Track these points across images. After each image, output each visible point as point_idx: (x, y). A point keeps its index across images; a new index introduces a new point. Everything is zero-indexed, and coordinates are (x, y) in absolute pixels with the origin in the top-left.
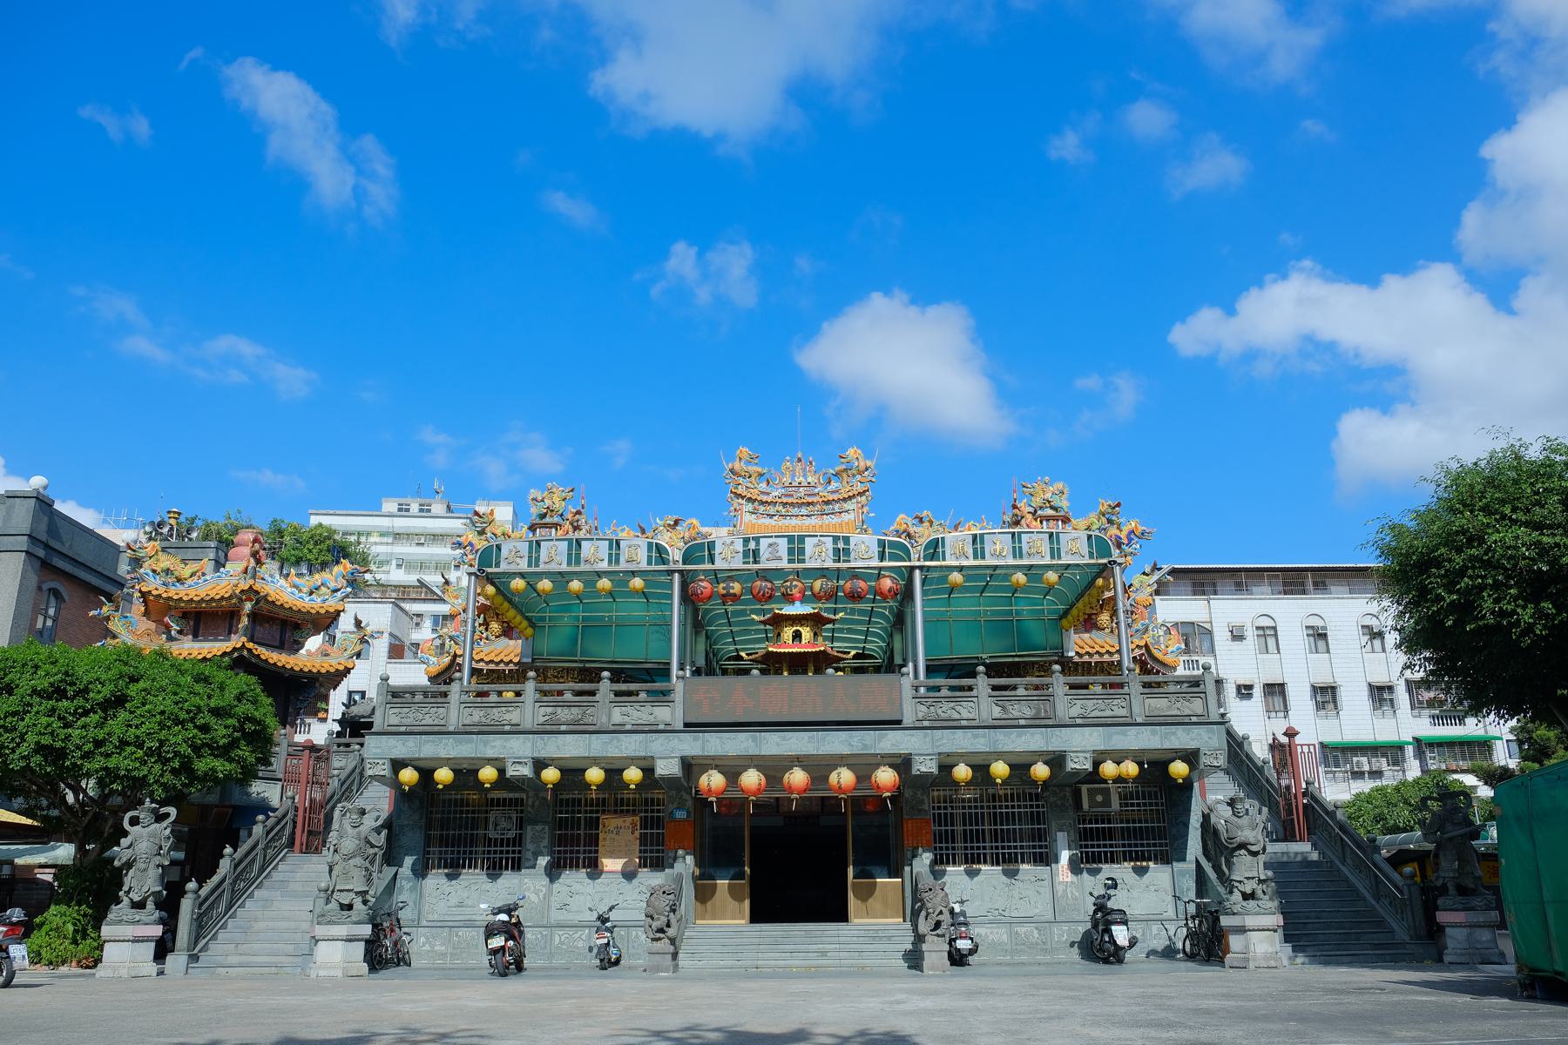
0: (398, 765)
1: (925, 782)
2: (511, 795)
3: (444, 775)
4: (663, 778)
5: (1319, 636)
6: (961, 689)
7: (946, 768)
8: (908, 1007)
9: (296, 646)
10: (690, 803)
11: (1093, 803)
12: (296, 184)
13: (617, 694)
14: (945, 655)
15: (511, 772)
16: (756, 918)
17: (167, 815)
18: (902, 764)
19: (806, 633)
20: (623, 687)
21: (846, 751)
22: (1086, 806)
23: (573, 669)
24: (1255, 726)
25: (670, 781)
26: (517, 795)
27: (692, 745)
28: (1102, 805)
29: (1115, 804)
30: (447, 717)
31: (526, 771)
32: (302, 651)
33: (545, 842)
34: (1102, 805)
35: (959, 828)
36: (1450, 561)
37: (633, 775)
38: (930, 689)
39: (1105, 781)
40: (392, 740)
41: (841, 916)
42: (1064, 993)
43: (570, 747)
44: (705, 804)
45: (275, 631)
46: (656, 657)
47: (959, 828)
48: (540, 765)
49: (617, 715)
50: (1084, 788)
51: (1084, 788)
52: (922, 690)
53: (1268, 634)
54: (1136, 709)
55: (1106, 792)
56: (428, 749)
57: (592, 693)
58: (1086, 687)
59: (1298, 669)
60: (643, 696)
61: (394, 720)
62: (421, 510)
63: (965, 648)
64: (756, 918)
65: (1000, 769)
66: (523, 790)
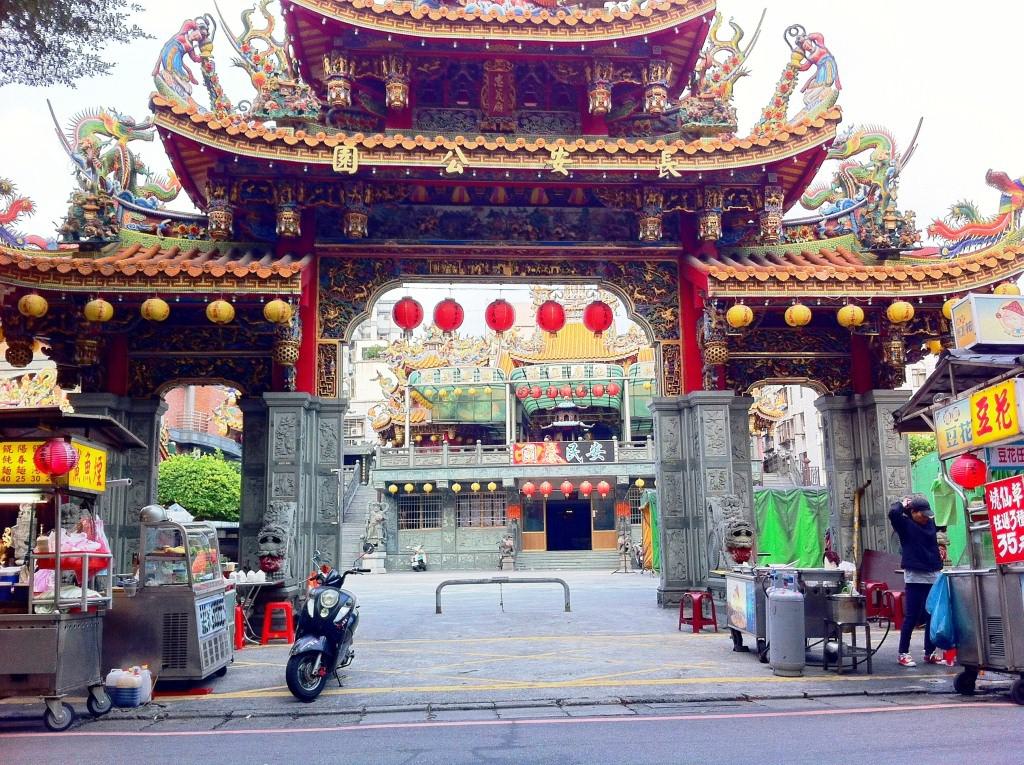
0: (388, 484)
1: (624, 487)
3: (409, 488)
5: (89, 455)
6: (640, 446)
7: (633, 479)
12: (12, 293)
13: (485, 450)
15: (439, 486)
16: (550, 548)
18: (612, 479)
19: (571, 416)
21: (588, 474)
25: (510, 489)
27: (518, 473)
30: (408, 462)
31: (446, 485)
33: (453, 516)
36: (899, 356)
37: (428, 487)
40: (385, 473)
41: (587, 546)
43: (465, 475)
48: (452, 482)
49: (485, 461)
54: (445, 461)
56: (401, 477)
57: (644, 445)
58: (459, 450)
60: (496, 450)
61: (385, 464)
64: (550, 548)
65: (409, 488)
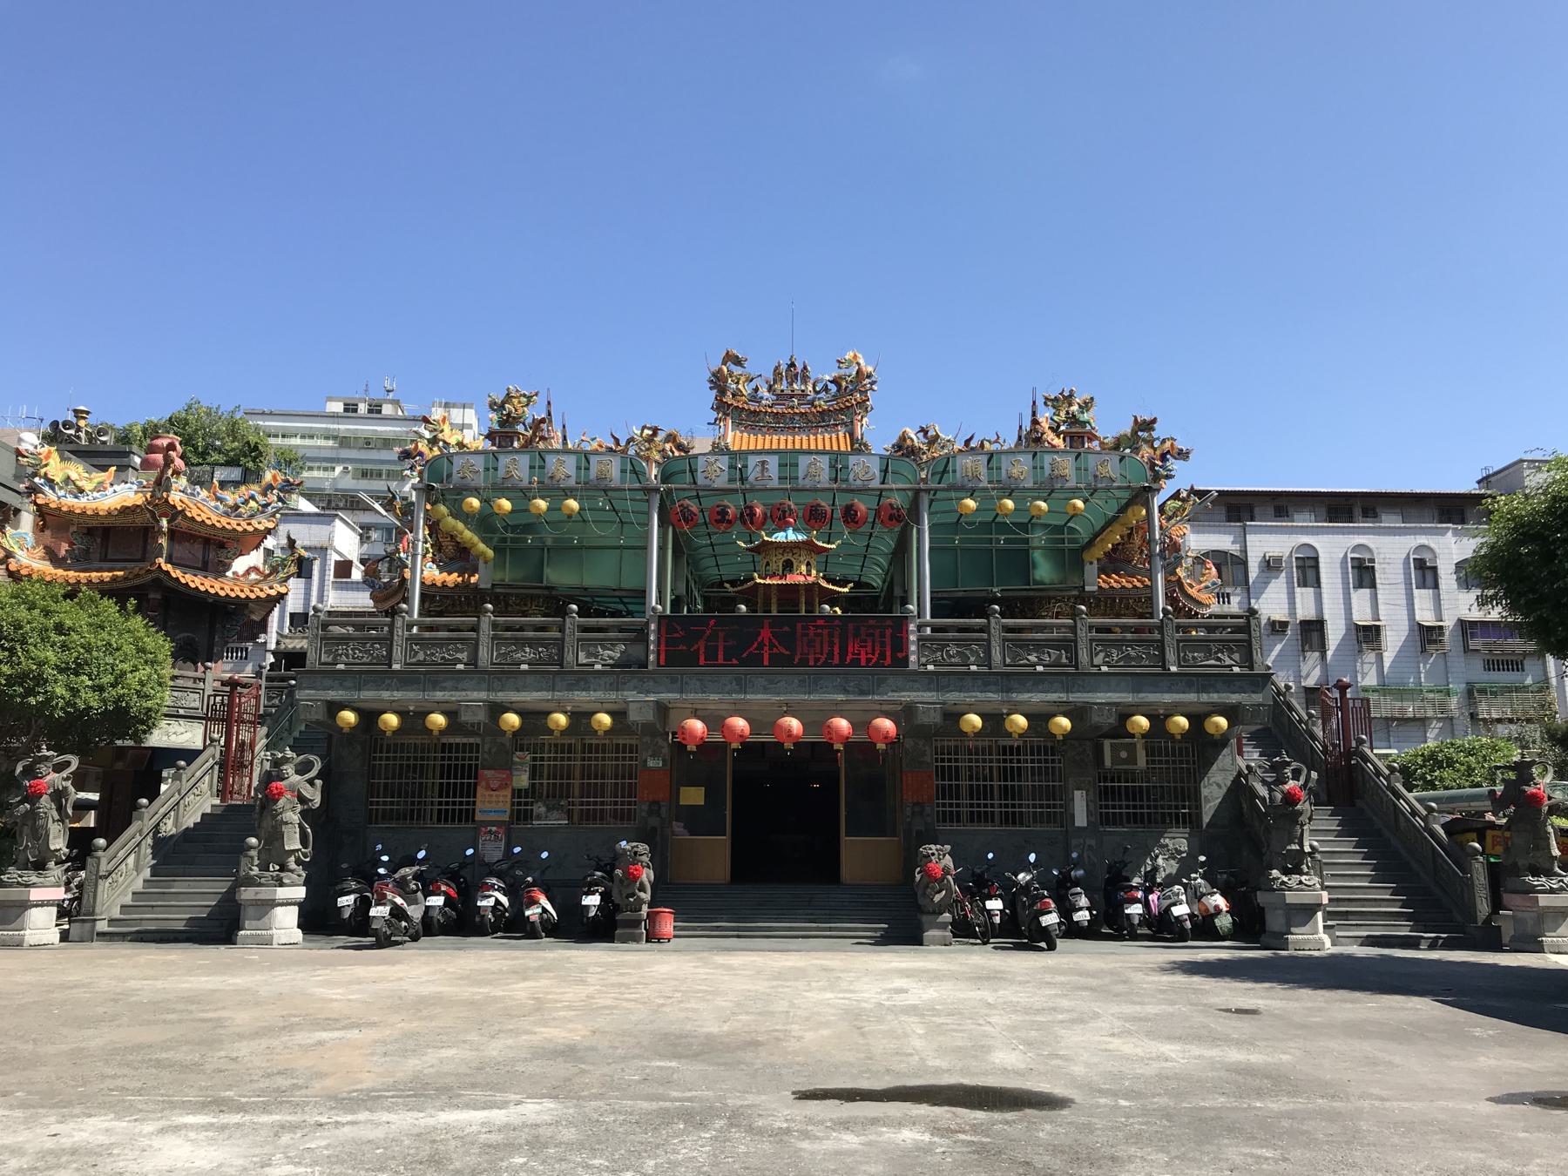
2: (465, 740)
4: (636, 723)
8: (911, 1000)
9: (220, 569)
10: (666, 750)
11: (1116, 759)
14: (960, 591)
17: (68, 764)
20: (592, 621)
22: (1108, 763)
23: (539, 596)
24: (1294, 674)
26: (472, 740)
28: (1125, 761)
29: (1142, 761)
31: (481, 716)
32: (229, 574)
34: (1125, 761)
35: (964, 783)
38: (423, 627)
39: (1133, 736)
42: (1083, 980)
44: (680, 747)
45: (198, 550)
46: (629, 583)
47: (964, 783)
50: (1107, 743)
51: (1107, 743)
52: (415, 630)
53: (1308, 569)
55: (1131, 749)
59: (1337, 607)
62: (370, 411)
63: (968, 587)
66: (477, 734)
